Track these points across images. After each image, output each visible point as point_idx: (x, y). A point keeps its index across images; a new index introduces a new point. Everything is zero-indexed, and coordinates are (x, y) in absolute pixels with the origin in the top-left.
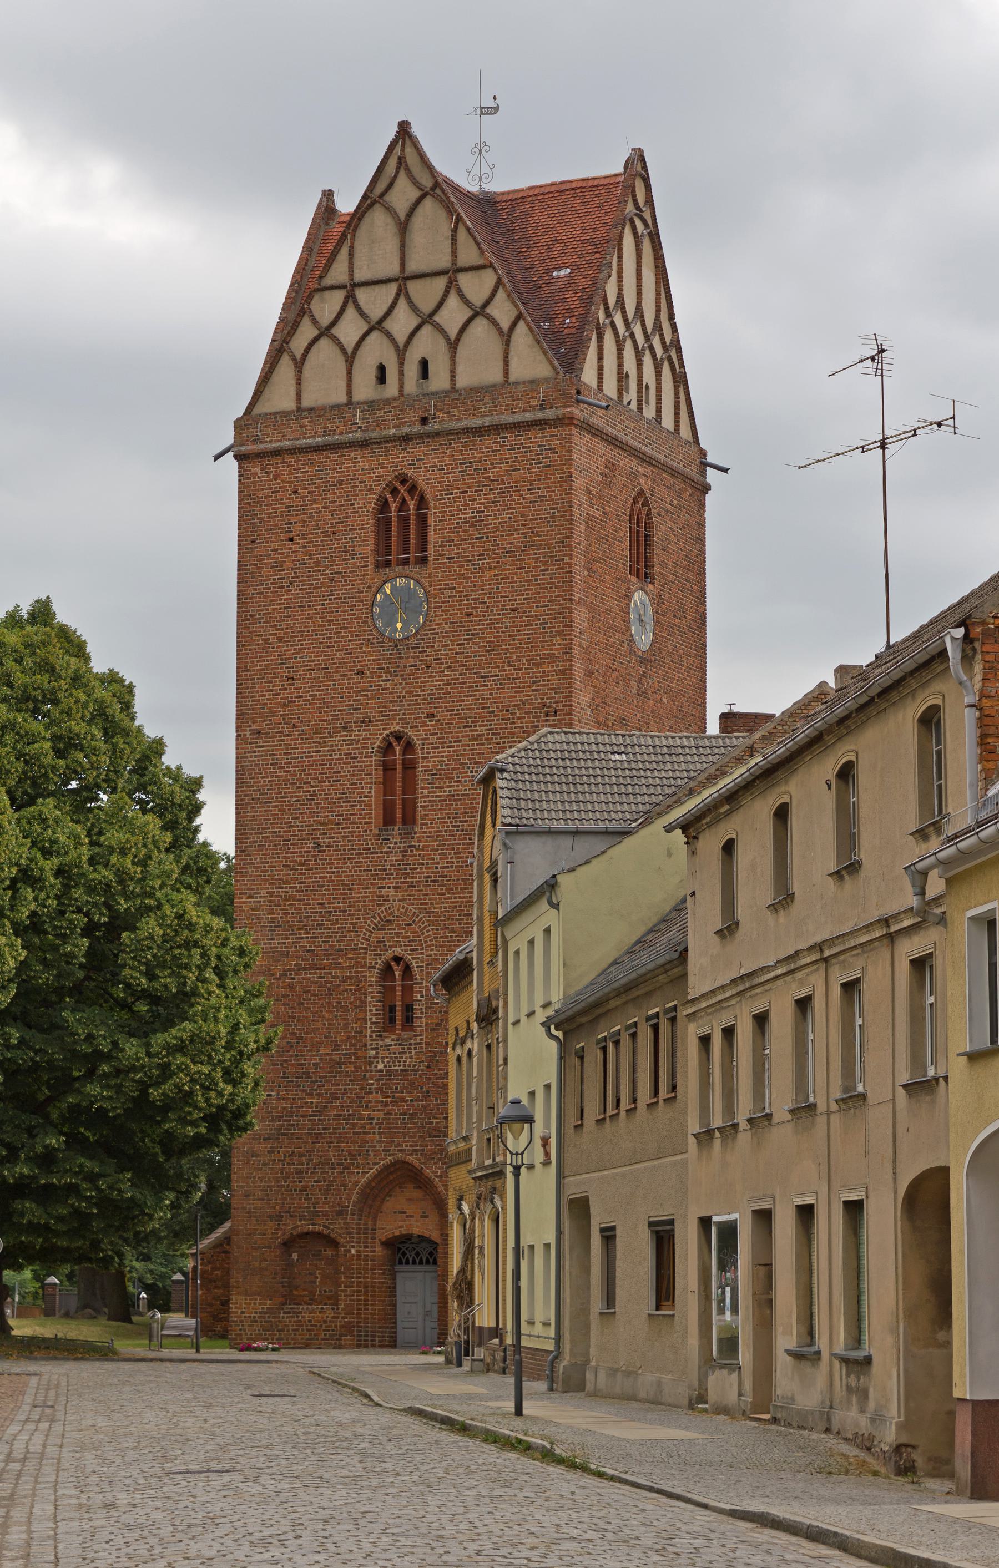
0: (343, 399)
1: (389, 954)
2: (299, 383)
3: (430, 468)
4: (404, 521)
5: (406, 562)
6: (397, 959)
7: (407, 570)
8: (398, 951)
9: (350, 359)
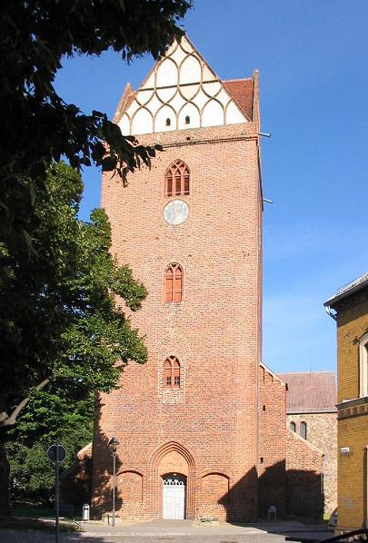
0: (151, 131)
1: (169, 355)
2: (225, 116)
3: (190, 155)
4: (178, 180)
5: (179, 194)
6: (172, 357)
7: (179, 197)
8: (173, 354)
9: (154, 117)
